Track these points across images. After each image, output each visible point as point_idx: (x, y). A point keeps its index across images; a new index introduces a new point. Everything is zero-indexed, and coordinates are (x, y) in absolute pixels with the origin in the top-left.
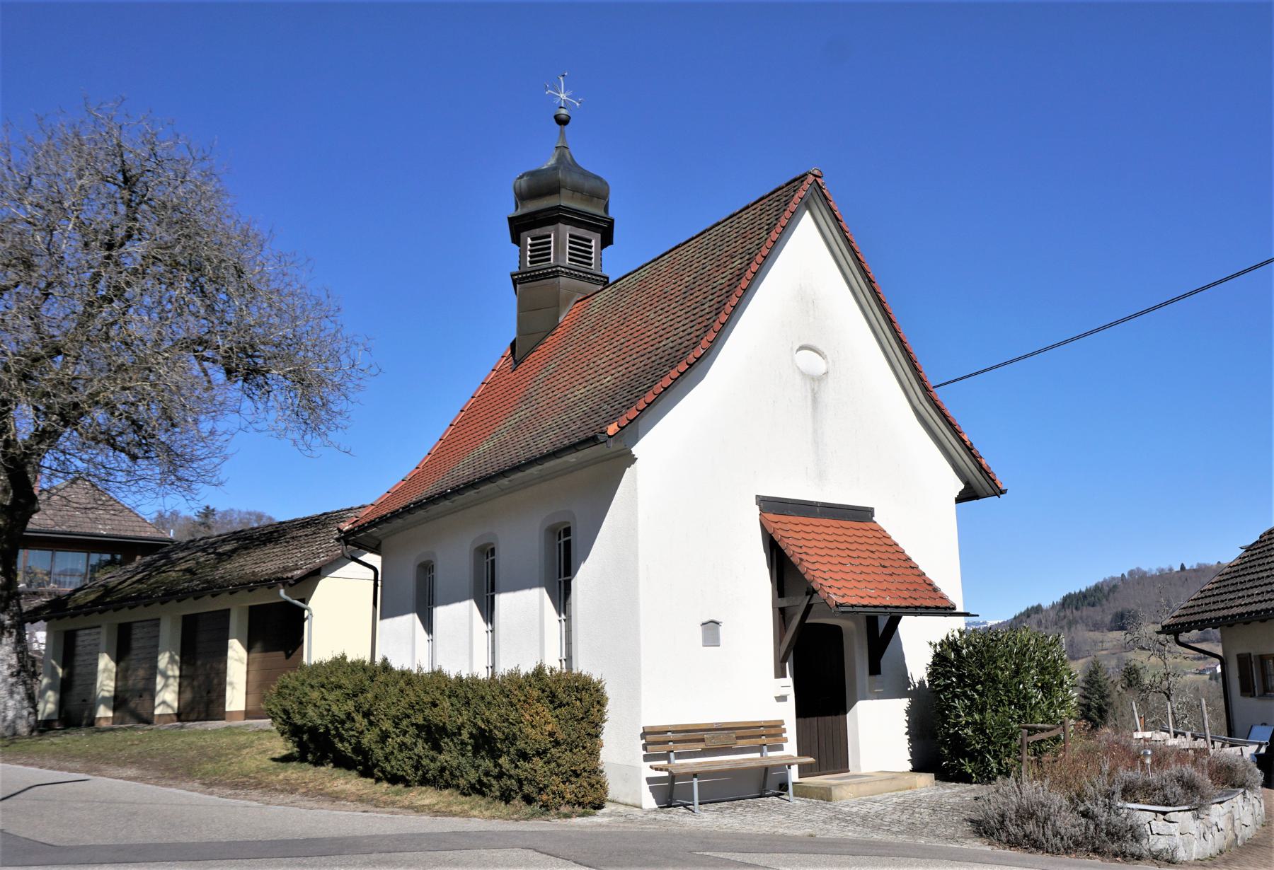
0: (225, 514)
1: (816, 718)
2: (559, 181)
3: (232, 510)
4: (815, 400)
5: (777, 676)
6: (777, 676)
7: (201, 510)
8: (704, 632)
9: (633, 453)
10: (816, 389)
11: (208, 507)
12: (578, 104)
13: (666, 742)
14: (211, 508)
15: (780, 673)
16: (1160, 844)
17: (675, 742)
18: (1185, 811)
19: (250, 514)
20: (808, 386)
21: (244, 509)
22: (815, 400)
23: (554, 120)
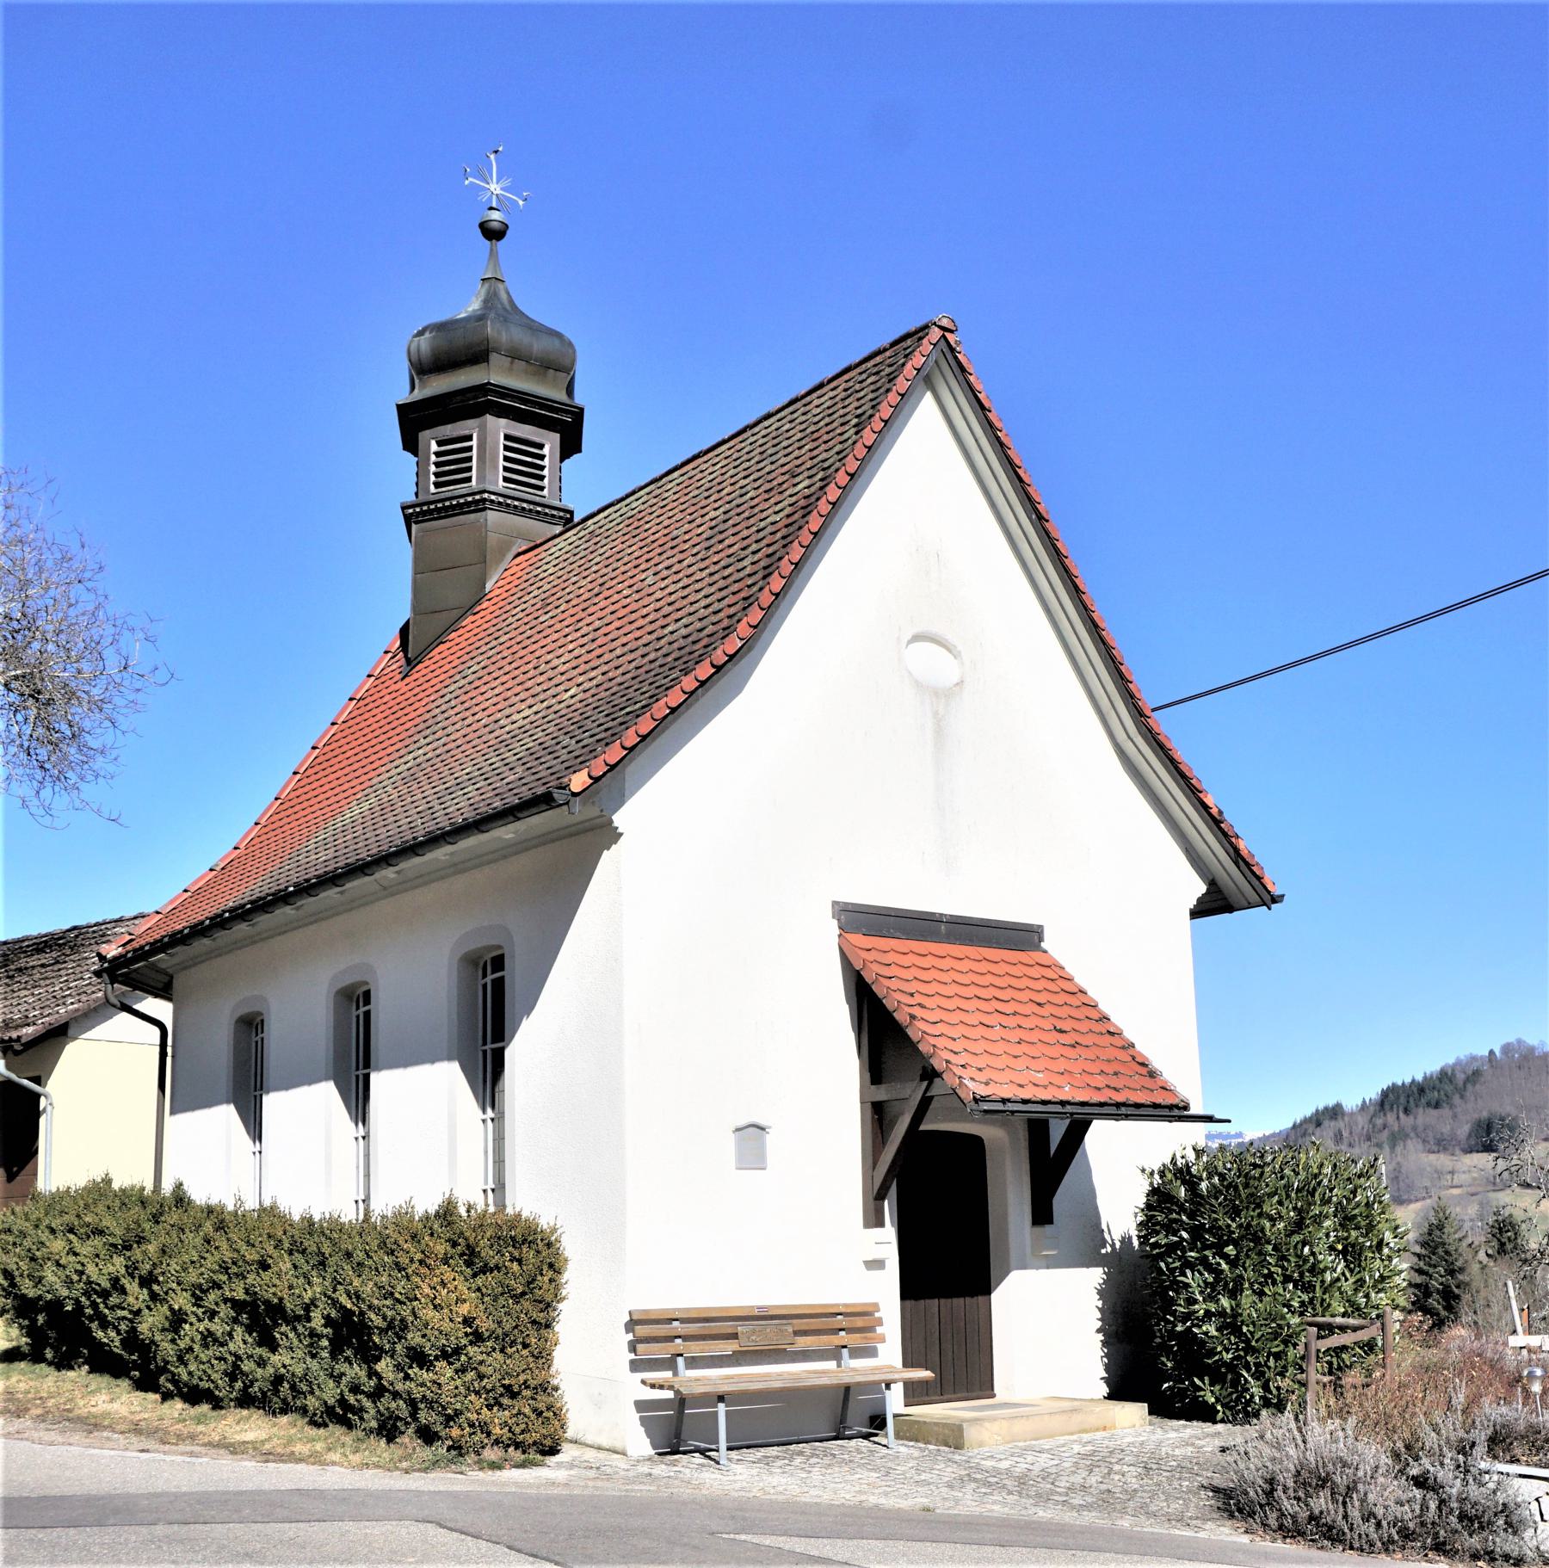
4: (940, 732)
12: (521, 203)
13: (671, 1339)
17: (685, 1338)
22: (940, 732)
23: (479, 231)
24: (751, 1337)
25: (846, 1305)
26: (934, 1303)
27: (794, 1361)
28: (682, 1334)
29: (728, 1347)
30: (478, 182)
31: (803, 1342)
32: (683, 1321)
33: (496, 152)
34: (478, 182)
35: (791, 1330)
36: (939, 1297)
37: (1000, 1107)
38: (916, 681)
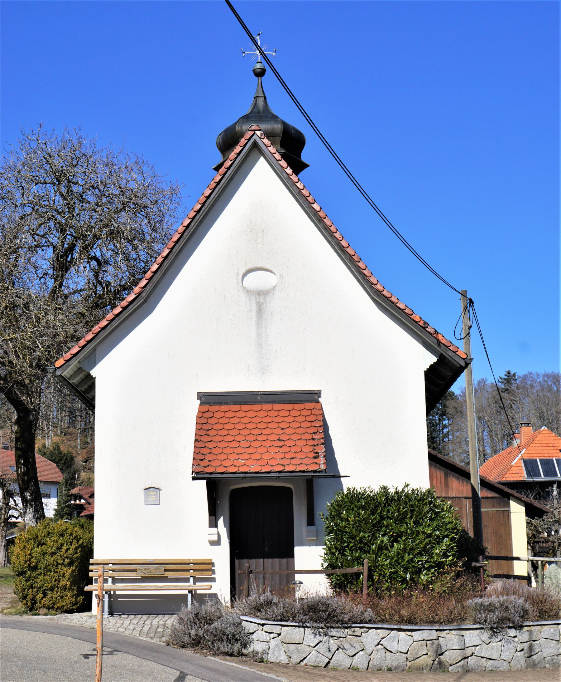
0: (525, 377)
1: (262, 560)
2: (236, 133)
3: (531, 373)
4: (260, 311)
5: (210, 526)
6: (210, 526)
7: (504, 377)
8: (146, 496)
9: (92, 375)
10: (261, 301)
11: (509, 373)
12: (274, 54)
13: (188, 570)
14: (512, 373)
15: (213, 524)
16: (256, 646)
17: (194, 570)
18: (296, 626)
19: (547, 376)
20: (253, 301)
21: (542, 372)
22: (260, 311)
23: (253, 73)
24: (153, 571)
25: (194, 560)
26: (277, 560)
27: (171, 582)
28: (193, 568)
29: (132, 576)
30: (250, 52)
31: (170, 575)
32: (113, 564)
33: (259, 34)
34: (250, 52)
35: (163, 569)
36: (264, 558)
37: (278, 475)
38: (247, 290)
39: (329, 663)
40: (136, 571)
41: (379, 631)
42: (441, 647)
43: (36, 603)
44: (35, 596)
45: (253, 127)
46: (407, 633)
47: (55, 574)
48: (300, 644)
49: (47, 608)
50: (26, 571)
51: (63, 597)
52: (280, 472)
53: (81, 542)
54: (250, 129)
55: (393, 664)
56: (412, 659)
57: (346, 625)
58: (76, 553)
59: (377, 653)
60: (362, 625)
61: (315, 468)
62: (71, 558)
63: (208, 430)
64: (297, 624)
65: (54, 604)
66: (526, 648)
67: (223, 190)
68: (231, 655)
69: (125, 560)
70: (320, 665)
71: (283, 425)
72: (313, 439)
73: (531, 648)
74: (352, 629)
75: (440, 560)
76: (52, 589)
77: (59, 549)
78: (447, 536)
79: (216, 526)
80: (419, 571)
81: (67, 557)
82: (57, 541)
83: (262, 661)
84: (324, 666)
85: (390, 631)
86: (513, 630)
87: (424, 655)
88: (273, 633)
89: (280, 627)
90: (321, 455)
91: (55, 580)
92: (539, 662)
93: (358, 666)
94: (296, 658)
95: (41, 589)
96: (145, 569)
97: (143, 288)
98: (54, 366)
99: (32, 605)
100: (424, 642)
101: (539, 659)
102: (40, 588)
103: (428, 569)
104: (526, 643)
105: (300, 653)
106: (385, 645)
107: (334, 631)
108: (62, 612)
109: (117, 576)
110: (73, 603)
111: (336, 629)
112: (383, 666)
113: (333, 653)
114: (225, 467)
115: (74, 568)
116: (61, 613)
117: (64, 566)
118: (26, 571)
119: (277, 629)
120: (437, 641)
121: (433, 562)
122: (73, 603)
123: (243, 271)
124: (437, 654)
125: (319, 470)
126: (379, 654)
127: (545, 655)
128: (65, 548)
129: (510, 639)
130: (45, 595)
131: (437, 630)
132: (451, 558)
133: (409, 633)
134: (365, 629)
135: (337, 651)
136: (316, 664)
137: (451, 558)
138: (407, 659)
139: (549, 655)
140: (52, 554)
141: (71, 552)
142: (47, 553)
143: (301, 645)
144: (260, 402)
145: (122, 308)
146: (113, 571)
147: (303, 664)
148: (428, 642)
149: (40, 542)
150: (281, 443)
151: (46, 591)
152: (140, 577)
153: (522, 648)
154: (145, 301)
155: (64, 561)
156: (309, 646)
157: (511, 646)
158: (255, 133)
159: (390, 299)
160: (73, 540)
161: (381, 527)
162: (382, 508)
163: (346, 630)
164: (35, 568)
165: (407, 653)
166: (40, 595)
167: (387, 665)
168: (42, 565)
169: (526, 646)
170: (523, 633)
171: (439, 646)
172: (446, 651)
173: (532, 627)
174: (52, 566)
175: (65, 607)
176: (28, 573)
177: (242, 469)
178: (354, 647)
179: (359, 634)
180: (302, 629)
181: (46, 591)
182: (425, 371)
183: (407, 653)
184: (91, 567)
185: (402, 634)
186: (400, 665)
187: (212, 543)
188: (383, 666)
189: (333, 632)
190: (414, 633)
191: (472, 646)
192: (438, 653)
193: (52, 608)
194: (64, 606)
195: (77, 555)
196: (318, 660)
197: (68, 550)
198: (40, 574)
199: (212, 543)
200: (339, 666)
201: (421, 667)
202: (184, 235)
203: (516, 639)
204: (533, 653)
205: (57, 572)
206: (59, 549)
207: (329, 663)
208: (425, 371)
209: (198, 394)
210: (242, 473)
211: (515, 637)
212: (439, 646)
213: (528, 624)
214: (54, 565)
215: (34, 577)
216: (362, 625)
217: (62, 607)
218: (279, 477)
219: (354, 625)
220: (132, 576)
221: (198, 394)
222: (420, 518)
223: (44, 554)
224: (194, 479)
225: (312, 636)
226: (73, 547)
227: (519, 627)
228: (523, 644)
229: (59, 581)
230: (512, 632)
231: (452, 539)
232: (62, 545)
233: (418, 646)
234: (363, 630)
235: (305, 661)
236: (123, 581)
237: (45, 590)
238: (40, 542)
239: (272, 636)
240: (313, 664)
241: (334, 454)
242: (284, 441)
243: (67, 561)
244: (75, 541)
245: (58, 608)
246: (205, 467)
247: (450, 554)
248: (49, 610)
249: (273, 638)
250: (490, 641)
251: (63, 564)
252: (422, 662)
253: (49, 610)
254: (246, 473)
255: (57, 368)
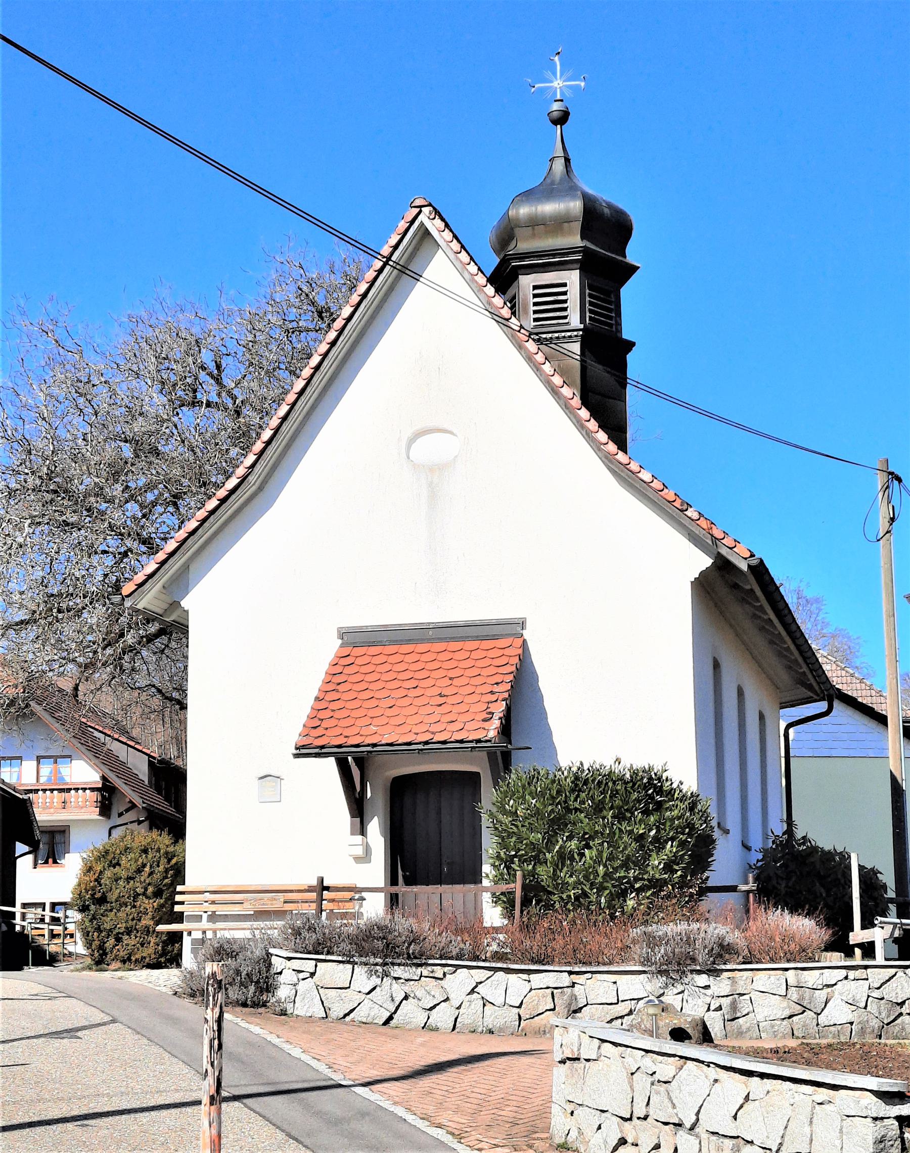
35: (282, 900)
39: (390, 1018)
40: (242, 903)
41: (473, 971)
42: (576, 999)
43: (105, 954)
44: (105, 943)
45: (416, 200)
46: (520, 975)
47: (133, 910)
48: (346, 988)
49: (121, 961)
50: (89, 905)
51: (144, 944)
52: (426, 743)
53: (174, 861)
54: (413, 205)
55: (495, 1023)
56: (528, 1017)
57: (417, 959)
58: (166, 877)
59: (470, 1005)
60: (444, 962)
61: (480, 735)
62: (156, 886)
63: (339, 684)
64: (340, 958)
65: (130, 955)
66: (725, 1006)
67: (379, 307)
68: (244, 1005)
69: (228, 886)
70: (376, 1021)
71: (452, 674)
72: (492, 692)
73: (734, 1007)
74: (430, 968)
75: (657, 876)
76: (129, 932)
77: (139, 871)
78: (673, 839)
79: (363, 832)
80: (623, 894)
81: (149, 884)
82: (136, 861)
83: (283, 1013)
84: (382, 1023)
85: (493, 972)
86: (704, 976)
87: (547, 1010)
88: (303, 971)
89: (314, 962)
90: (497, 715)
91: (133, 919)
92: (748, 1029)
93: (438, 1025)
94: (338, 1010)
95: (112, 932)
96: (256, 900)
97: (249, 468)
98: (121, 594)
99: (101, 955)
100: (549, 991)
101: (748, 1024)
102: (110, 930)
103: (639, 891)
104: (725, 998)
105: (344, 1003)
106: (483, 994)
107: (399, 970)
108: (143, 966)
109: (221, 910)
110: (158, 952)
111: (402, 967)
112: (479, 1026)
113: (397, 1003)
114: (346, 737)
115: (162, 901)
116: (142, 969)
117: (147, 897)
118: (89, 905)
119: (309, 966)
120: (569, 990)
121: (648, 880)
122: (158, 952)
123: (408, 433)
124: (569, 1011)
125: (486, 738)
126: (473, 1007)
127: (760, 1017)
128: (147, 869)
129: (697, 990)
130: (118, 940)
131: (570, 973)
132: (679, 873)
133: (525, 976)
134: (450, 968)
135: (404, 1001)
136: (369, 1020)
137: (679, 873)
138: (519, 1016)
139: (767, 1019)
140: (129, 879)
141: (157, 876)
142: (121, 878)
143: (348, 990)
144: (430, 640)
145: (218, 500)
146: (213, 902)
147: (348, 1019)
148: (555, 991)
149: (111, 862)
150: (442, 700)
151: (120, 936)
152: (252, 913)
153: (717, 1005)
154: (260, 489)
155: (146, 889)
156: (360, 992)
157: (700, 1002)
158: (420, 212)
159: (628, 466)
160: (160, 857)
161: (566, 825)
162: (566, 794)
163: (419, 969)
164: (103, 900)
165: (520, 1007)
166: (111, 941)
167: (485, 1025)
168: (112, 897)
169: (726, 1002)
170: (720, 981)
171: (573, 998)
172: (585, 1006)
173: (736, 972)
174: (128, 898)
175: (148, 959)
176: (92, 907)
177: (369, 741)
178: (434, 996)
179: (441, 976)
180: (350, 966)
181: (120, 936)
182: (692, 582)
183: (520, 1007)
184: (178, 898)
185: (513, 977)
186: (508, 1024)
187: (358, 859)
188: (479, 1026)
189: (398, 971)
190: (533, 977)
191: (631, 1000)
192: (572, 1009)
193: (127, 961)
194: (145, 958)
195: (166, 881)
196: (372, 1014)
197: (151, 874)
198: (111, 910)
199: (358, 859)
200: (408, 1023)
201: (542, 1029)
202: (312, 381)
203: (709, 992)
204: (738, 1015)
205: (134, 907)
206: (139, 871)
207: (390, 1018)
208: (692, 582)
209: (339, 629)
210: (368, 745)
211: (707, 987)
212: (574, 998)
213: (728, 967)
214: (130, 896)
215: (102, 915)
216: (444, 962)
217: (142, 960)
218: (422, 750)
219: (431, 961)
220: (235, 910)
221: (339, 629)
222: (627, 810)
223: (116, 880)
224: (297, 756)
225: (365, 976)
226: (161, 868)
227: (714, 972)
228: (720, 998)
229: (139, 920)
230: (702, 980)
231: (682, 844)
232: (144, 866)
233: (538, 997)
234: (446, 969)
235: (352, 1015)
236: (226, 918)
237: (119, 933)
238: (111, 862)
239: (302, 976)
240: (364, 1020)
241: (547, 718)
242: (447, 696)
243: (150, 889)
244: (163, 861)
245: (136, 960)
246: (316, 738)
247: (676, 867)
248: (124, 964)
249: (303, 979)
250: (662, 992)
251: (144, 894)
252: (544, 1022)
253: (124, 964)
254: (375, 745)
255: (126, 596)
